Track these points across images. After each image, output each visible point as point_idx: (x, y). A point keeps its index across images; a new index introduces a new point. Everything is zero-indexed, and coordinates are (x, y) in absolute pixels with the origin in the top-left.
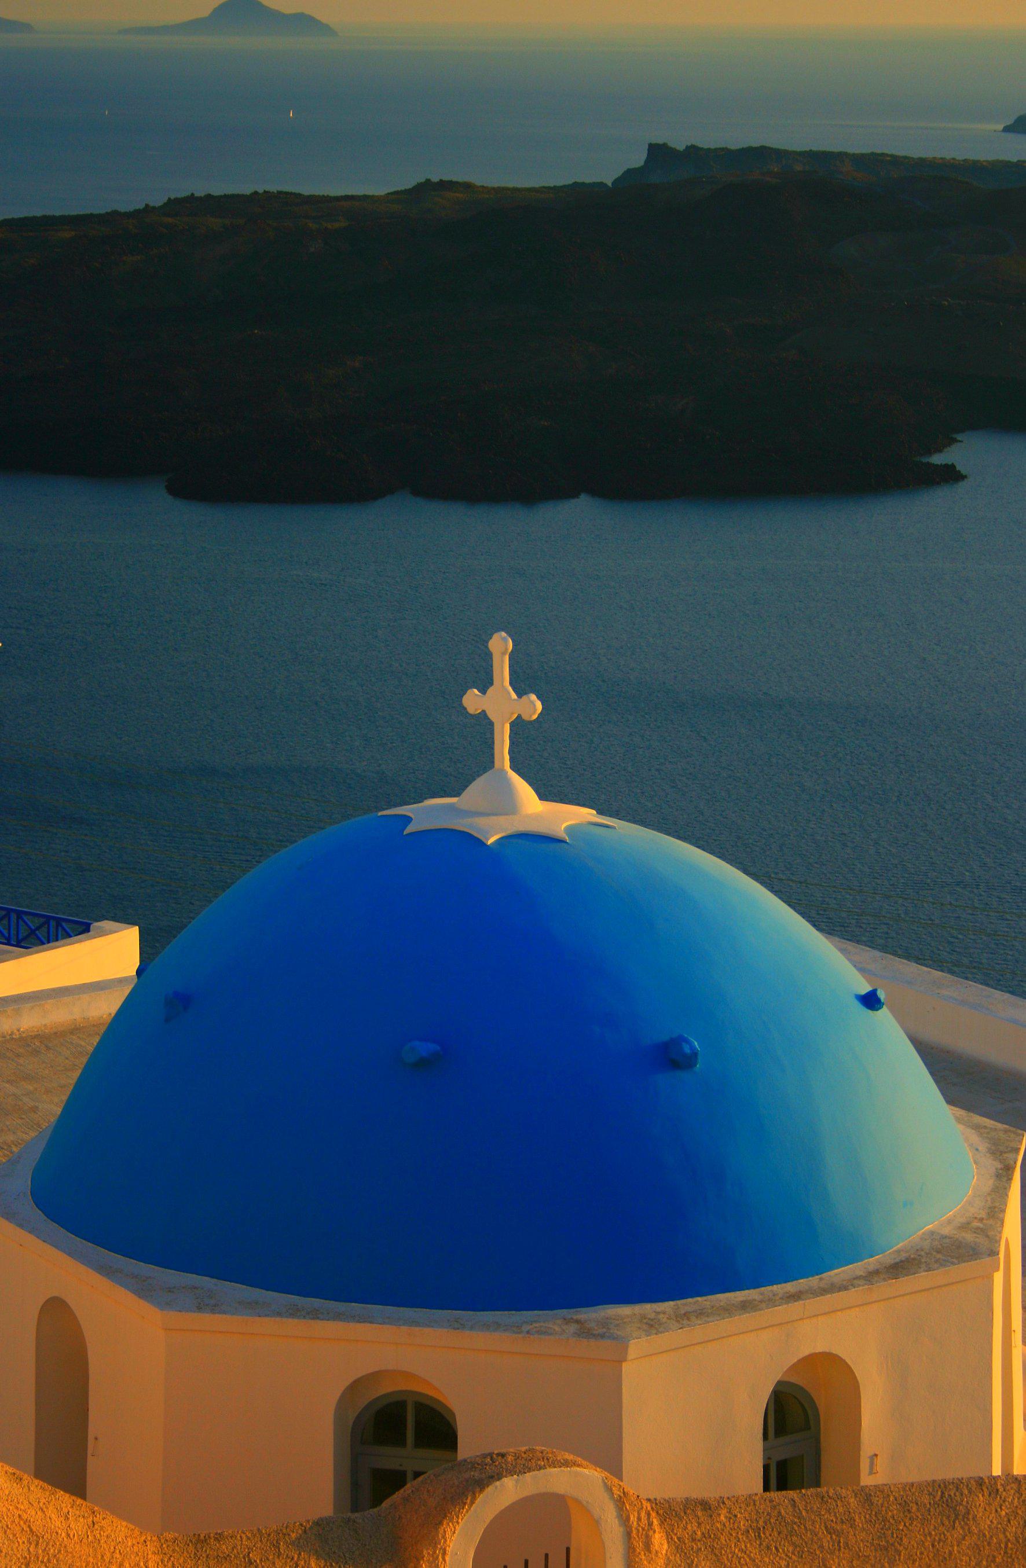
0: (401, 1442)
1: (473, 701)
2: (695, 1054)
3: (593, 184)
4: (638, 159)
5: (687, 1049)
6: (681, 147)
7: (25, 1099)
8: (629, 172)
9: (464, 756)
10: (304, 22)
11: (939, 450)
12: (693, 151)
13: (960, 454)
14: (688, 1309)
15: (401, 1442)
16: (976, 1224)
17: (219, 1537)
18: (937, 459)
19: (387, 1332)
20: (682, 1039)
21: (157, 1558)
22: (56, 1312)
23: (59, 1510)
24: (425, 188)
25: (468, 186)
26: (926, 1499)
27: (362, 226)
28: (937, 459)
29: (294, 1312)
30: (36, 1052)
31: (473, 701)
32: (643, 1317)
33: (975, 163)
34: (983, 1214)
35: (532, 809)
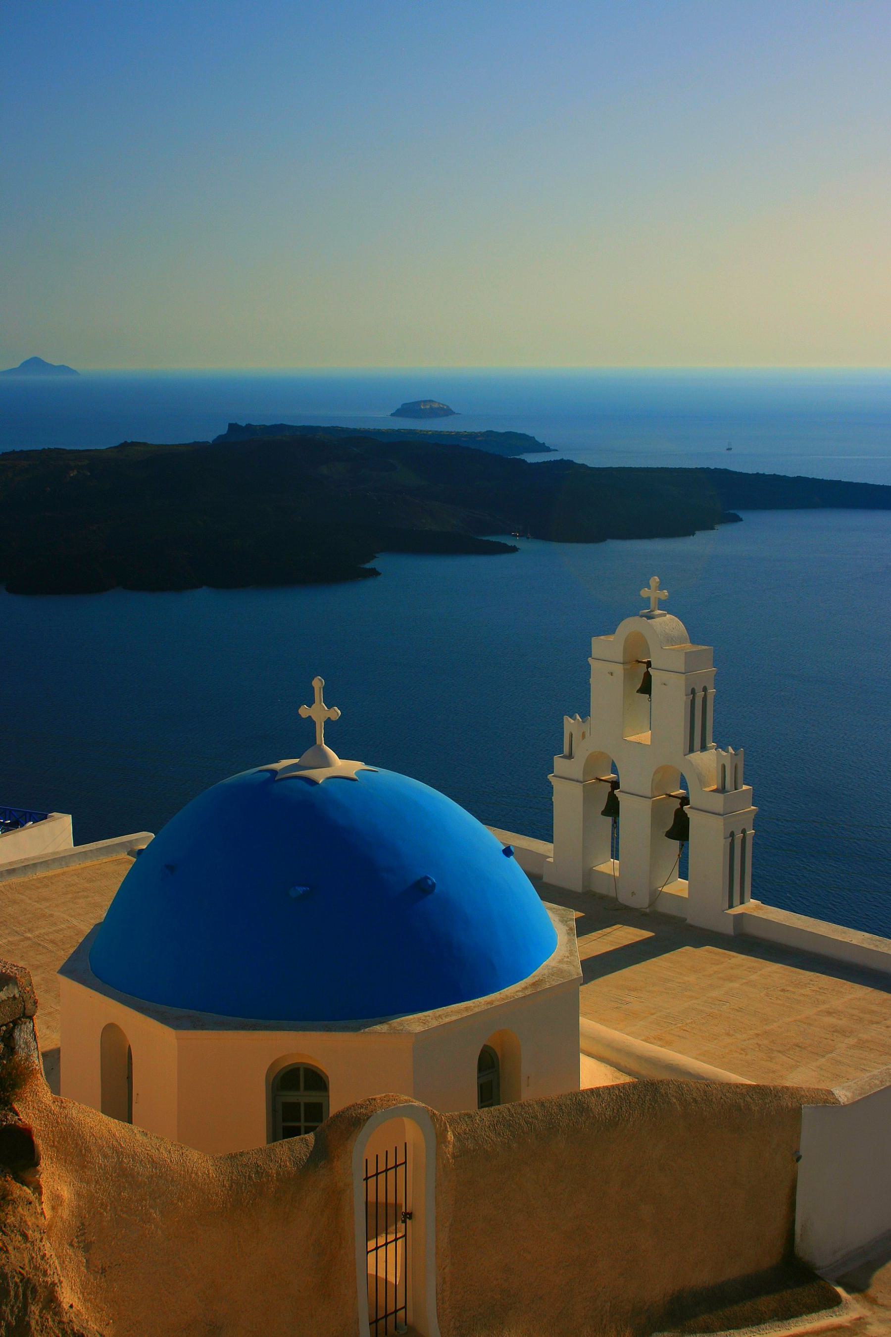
0: (298, 1089)
1: (304, 711)
2: (434, 884)
3: (204, 443)
4: (223, 430)
5: (430, 882)
6: (244, 424)
7: (46, 910)
8: (220, 437)
9: (300, 739)
10: (64, 369)
11: (368, 562)
12: (249, 426)
13: (378, 563)
14: (440, 1013)
15: (298, 1089)
16: (566, 959)
17: (242, 1154)
18: (368, 566)
19: (292, 1034)
20: (427, 878)
21: (213, 1168)
22: (111, 1032)
23: (166, 1149)
24: (125, 445)
25: (145, 444)
26: (569, 1102)
27: (93, 461)
28: (368, 566)
29: (243, 1027)
30: (46, 886)
31: (304, 711)
32: (419, 1019)
33: (379, 430)
34: (567, 954)
35: (344, 767)
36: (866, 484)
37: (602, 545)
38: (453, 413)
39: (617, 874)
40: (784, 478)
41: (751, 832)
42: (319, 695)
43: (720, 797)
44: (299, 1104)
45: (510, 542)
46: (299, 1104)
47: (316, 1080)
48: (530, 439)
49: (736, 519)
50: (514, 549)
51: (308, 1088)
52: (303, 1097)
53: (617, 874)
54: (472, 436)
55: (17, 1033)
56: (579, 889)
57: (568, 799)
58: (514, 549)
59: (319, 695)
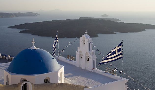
1: (32, 42)
13: (98, 35)
31: (32, 42)
36: (59, 20)
41: (96, 60)
42: (33, 40)
50: (116, 33)
56: (79, 67)
57: (78, 57)
58: (116, 33)
59: (33, 40)
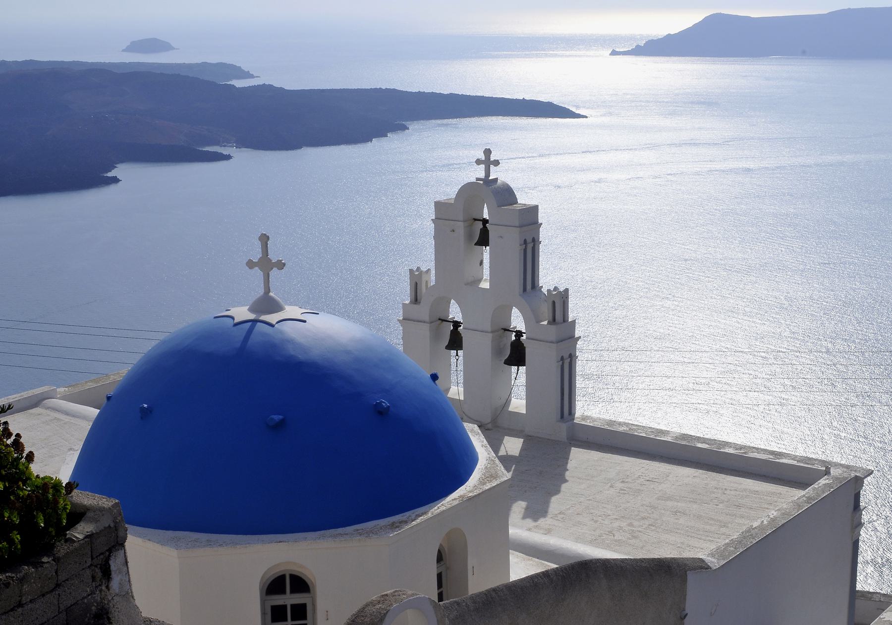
13: (120, 171)
18: (110, 174)
28: (110, 174)
37: (299, 152)
38: (173, 48)
39: (462, 398)
40: (440, 95)
43: (553, 327)
44: (285, 607)
45: (225, 151)
46: (285, 607)
47: (300, 584)
48: (245, 68)
49: (405, 128)
50: (228, 157)
51: (293, 591)
52: (289, 599)
53: (462, 398)
54: (190, 66)
55: (111, 562)
